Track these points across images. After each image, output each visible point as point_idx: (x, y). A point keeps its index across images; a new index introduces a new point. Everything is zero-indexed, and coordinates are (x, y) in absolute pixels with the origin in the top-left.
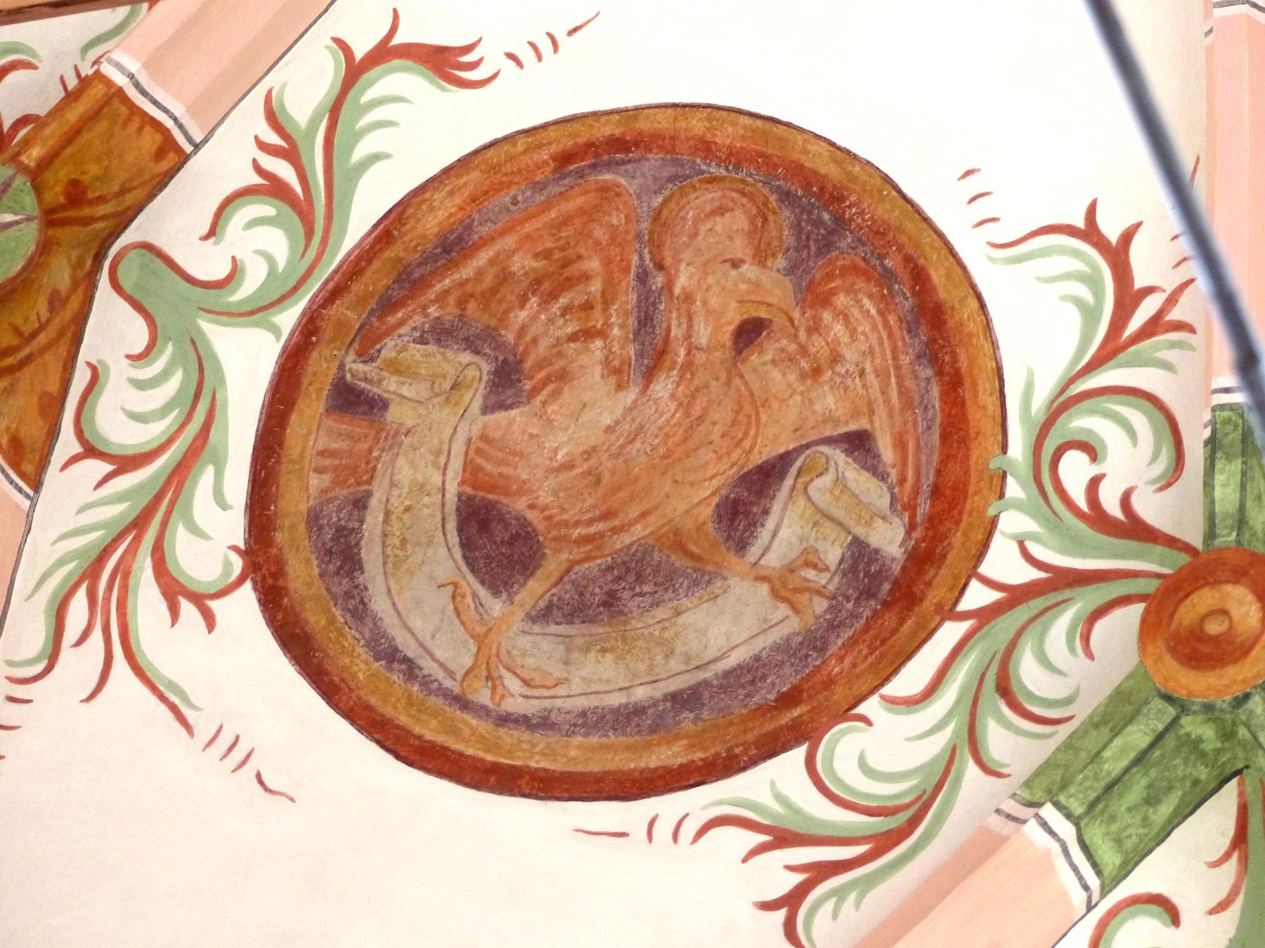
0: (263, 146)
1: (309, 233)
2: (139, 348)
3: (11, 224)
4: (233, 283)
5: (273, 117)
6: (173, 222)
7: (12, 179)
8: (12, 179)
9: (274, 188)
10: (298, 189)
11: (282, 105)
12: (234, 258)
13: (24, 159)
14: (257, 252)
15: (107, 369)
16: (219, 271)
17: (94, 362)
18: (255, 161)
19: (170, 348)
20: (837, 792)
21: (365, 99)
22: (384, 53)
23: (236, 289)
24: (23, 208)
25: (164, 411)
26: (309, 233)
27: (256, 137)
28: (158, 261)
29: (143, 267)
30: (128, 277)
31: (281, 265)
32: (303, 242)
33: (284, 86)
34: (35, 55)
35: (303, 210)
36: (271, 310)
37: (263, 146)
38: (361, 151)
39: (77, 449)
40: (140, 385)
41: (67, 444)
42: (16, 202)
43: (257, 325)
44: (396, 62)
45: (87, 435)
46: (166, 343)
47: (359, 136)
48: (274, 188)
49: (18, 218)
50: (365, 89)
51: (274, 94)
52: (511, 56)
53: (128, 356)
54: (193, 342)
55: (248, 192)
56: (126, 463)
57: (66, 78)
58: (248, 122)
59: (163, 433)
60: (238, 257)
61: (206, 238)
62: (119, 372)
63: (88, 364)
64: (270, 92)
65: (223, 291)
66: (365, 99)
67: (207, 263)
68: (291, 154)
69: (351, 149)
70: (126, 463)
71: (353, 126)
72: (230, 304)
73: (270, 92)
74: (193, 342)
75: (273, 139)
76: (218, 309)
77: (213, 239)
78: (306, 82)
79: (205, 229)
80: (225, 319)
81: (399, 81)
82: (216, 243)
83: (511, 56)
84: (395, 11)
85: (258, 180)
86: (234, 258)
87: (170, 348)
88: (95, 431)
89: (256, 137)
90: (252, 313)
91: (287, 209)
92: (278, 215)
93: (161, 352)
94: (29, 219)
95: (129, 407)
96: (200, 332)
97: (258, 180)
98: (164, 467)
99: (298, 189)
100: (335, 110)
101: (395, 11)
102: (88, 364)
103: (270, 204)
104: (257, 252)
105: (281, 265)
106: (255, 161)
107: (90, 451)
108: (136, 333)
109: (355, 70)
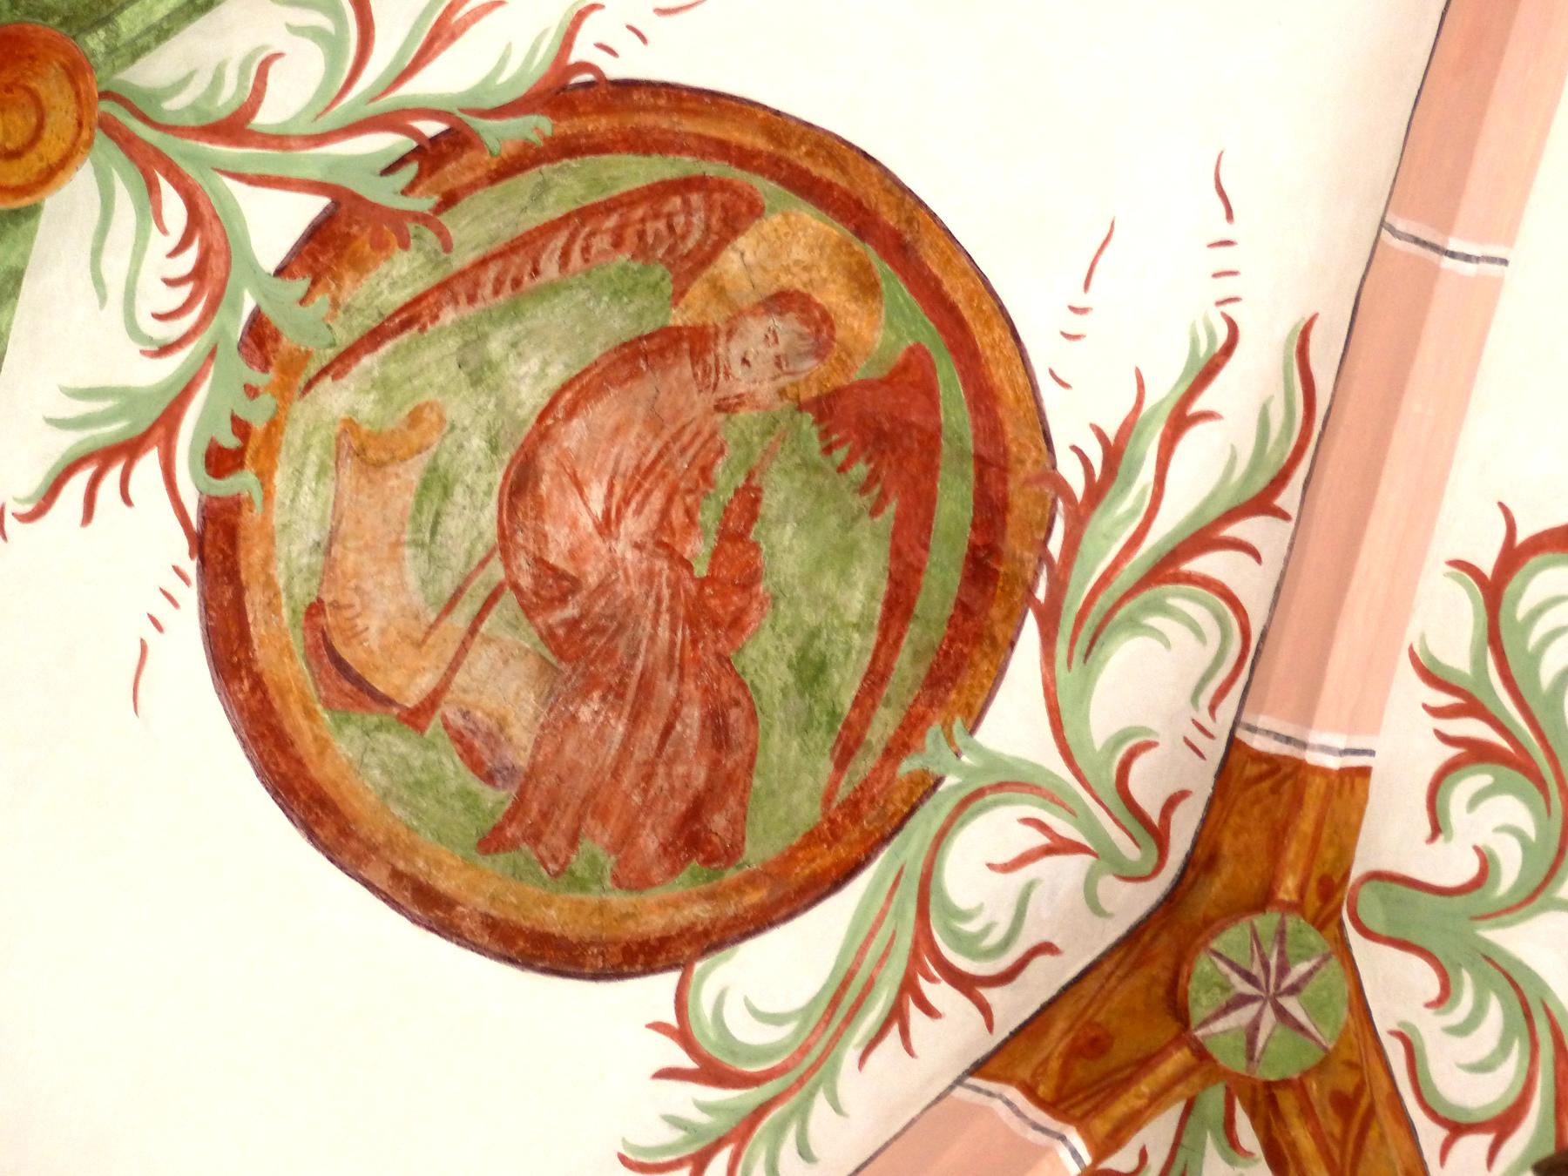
0: (1437, 712)
1: (1541, 785)
2: (1434, 990)
3: (1310, 973)
4: (1491, 875)
5: (1431, 676)
6: (1390, 837)
7: (1282, 923)
8: (1282, 923)
9: (1475, 753)
10: (1504, 743)
11: (1431, 657)
12: (1476, 849)
13: (1282, 895)
14: (1498, 830)
15: (1414, 1029)
16: (1470, 869)
17: (1396, 1028)
18: (1438, 733)
19: (1467, 978)
20: (1230, 613)
21: (1522, 611)
22: (1514, 556)
23: (1497, 882)
24: (1313, 949)
25: (1504, 1049)
26: (1541, 785)
27: (1425, 707)
28: (96, 213)
29: (1384, 900)
30: (1373, 915)
31: (1531, 832)
32: (1540, 798)
33: (1423, 638)
34: (1148, 731)
35: (1520, 762)
36: (1550, 886)
37: (1437, 712)
38: (1548, 672)
39: (1441, 1133)
40: (1462, 1030)
41: (1430, 1135)
42: (1301, 946)
43: (1544, 908)
44: (1533, 561)
45: (1442, 1113)
46: (1458, 973)
47: (1535, 658)
48: (1475, 753)
49: (1313, 962)
50: (1515, 604)
51: (1417, 649)
52: (1084, 311)
53: (1428, 1005)
54: (1488, 959)
55: (1447, 771)
56: (1503, 1124)
57: (1191, 738)
58: (1411, 695)
59: (1518, 1073)
60: (1480, 844)
61: (1433, 837)
62: (1430, 1028)
63: (1392, 1033)
64: (1411, 650)
65: (1486, 886)
66: (1522, 611)
67: (1450, 865)
68: (1472, 707)
69: (1536, 675)
70: (1503, 1124)
71: (1524, 649)
72: (1501, 899)
73: (1411, 650)
74: (1488, 959)
75: (1443, 699)
76: (1492, 910)
77: (1441, 838)
78: (1449, 626)
79: (1427, 829)
80: (1506, 918)
81: (1547, 581)
82: (1448, 839)
83: (1084, 311)
84: (1501, 505)
85: (1452, 752)
86: (1476, 849)
87: (1467, 978)
88: (1447, 1105)
89: (1425, 707)
90: (1531, 898)
91: (1504, 770)
92: (1496, 779)
93: (1460, 984)
94: (1326, 958)
95: (1466, 1061)
96: (1488, 944)
97: (1452, 752)
98: (1543, 1112)
99: (1504, 743)
100: (1494, 638)
101: (1501, 505)
102: (1392, 1033)
103: (1481, 772)
104: (1498, 830)
105: (1531, 832)
106: (1438, 733)
107: (1457, 1129)
108: (1421, 978)
109: (1493, 590)
